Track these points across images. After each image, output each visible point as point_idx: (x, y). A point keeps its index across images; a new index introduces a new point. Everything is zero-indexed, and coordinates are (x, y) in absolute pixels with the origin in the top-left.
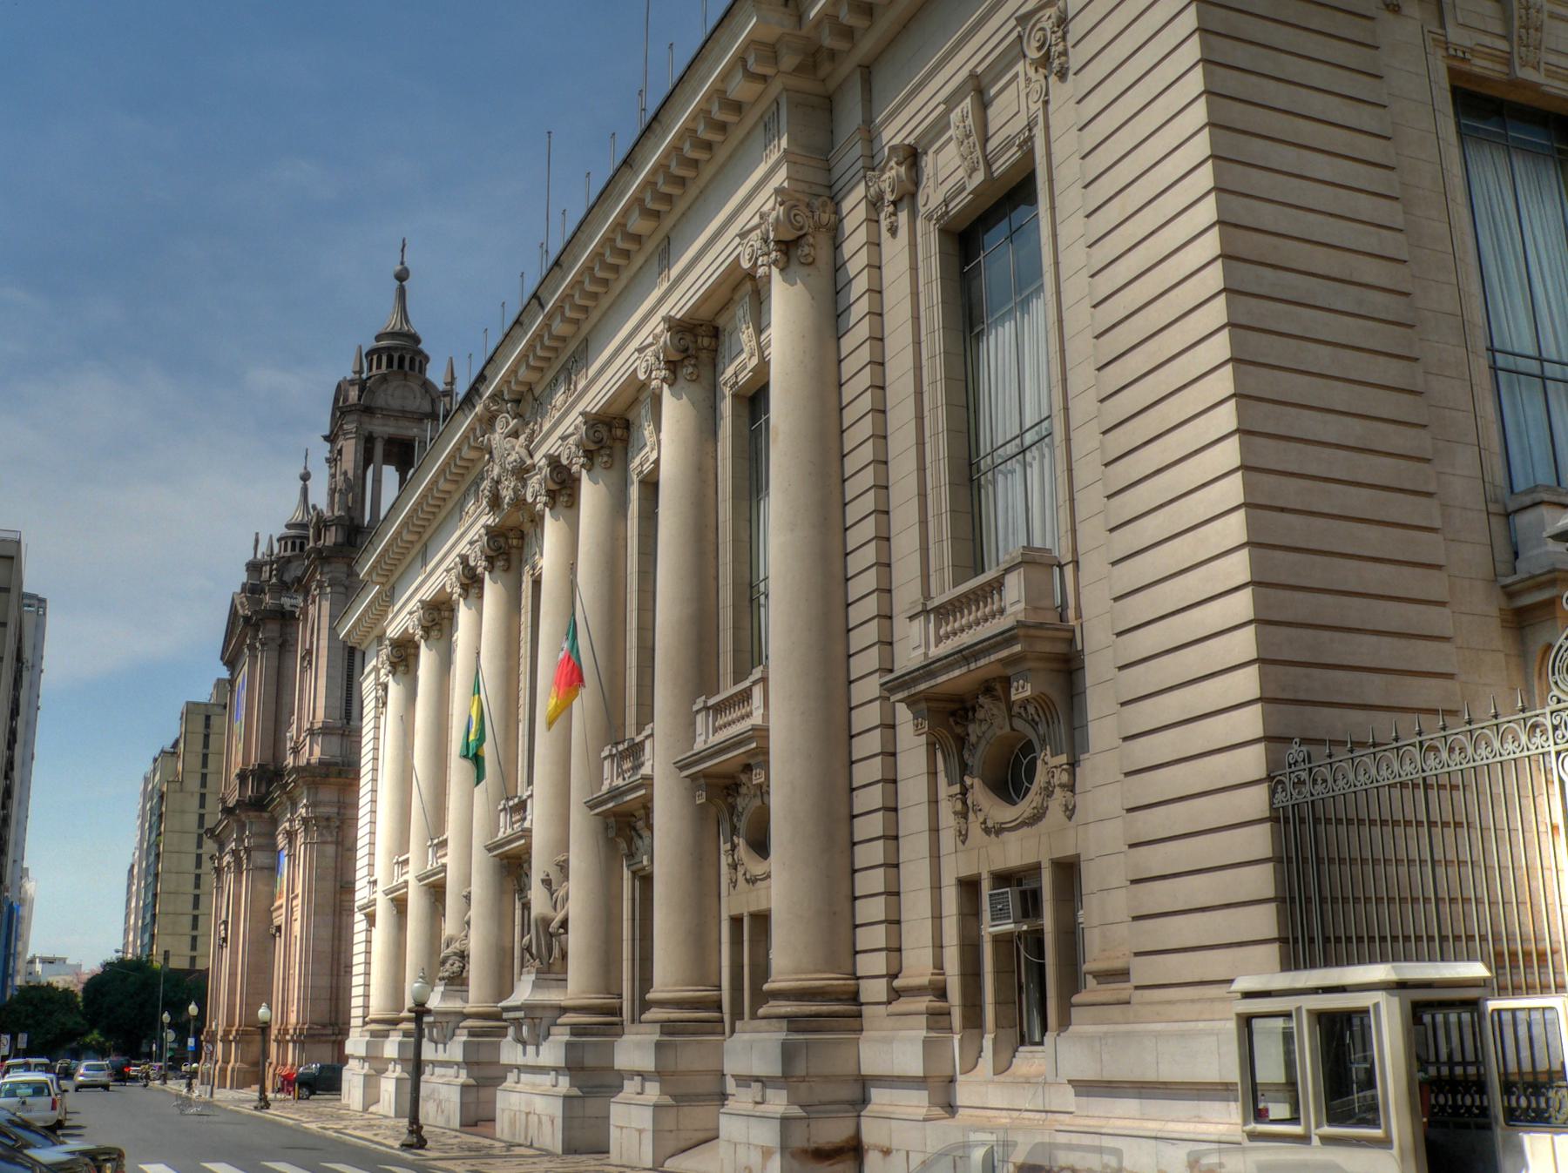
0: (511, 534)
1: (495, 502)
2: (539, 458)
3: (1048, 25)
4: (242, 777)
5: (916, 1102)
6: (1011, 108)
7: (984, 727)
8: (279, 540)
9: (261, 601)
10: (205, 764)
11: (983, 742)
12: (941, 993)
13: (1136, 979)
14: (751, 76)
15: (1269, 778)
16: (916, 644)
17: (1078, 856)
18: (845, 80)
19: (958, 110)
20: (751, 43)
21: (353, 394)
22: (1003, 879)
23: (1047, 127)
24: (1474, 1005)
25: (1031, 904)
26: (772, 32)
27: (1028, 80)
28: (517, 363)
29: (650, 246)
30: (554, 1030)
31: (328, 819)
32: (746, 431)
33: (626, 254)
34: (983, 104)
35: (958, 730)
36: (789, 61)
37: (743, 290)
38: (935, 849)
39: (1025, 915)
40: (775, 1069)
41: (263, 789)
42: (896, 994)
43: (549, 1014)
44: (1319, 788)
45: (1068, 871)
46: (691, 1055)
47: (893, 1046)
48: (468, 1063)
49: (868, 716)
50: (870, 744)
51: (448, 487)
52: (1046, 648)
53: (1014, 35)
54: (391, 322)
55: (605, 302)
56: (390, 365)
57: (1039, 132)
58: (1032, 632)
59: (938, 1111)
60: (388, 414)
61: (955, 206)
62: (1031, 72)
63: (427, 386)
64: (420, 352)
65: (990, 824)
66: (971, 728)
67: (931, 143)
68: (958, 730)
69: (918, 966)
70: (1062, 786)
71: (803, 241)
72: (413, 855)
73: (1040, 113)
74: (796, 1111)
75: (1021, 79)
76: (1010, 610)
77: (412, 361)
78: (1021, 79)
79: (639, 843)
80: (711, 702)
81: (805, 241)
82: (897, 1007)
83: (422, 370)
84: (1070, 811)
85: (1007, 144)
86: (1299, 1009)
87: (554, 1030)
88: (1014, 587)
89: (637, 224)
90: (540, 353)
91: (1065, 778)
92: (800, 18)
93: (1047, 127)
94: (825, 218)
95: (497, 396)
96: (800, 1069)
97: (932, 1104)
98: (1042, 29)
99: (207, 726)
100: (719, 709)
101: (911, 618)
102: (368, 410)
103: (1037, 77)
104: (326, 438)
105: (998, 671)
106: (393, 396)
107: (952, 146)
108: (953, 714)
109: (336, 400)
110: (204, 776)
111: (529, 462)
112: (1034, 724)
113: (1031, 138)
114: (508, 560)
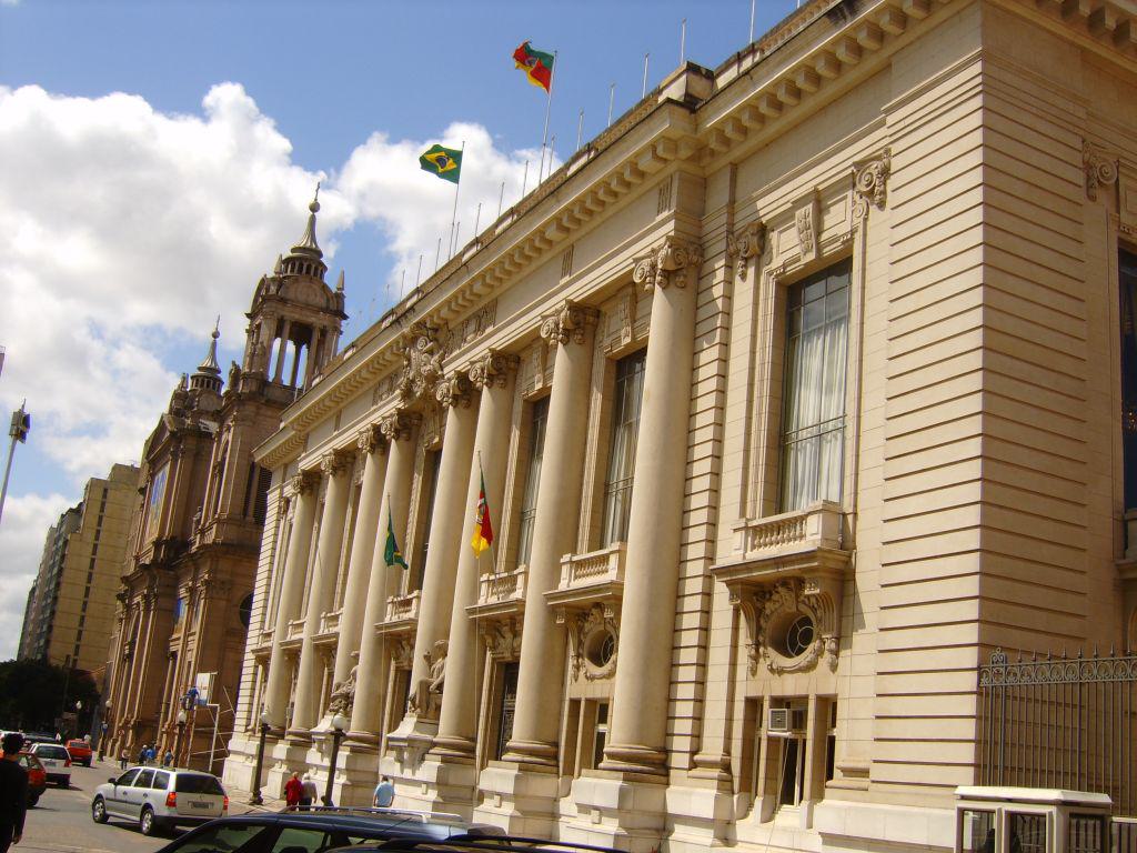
0: (414, 416)
1: (407, 394)
2: (449, 371)
3: (875, 173)
4: (157, 544)
5: (705, 836)
6: (839, 220)
7: (777, 605)
8: (192, 377)
9: (184, 423)
10: (99, 524)
11: (776, 614)
12: (727, 767)
13: (873, 776)
14: (656, 157)
15: (979, 668)
16: (732, 550)
17: (836, 695)
18: (719, 170)
19: (803, 210)
20: (662, 137)
21: (273, 289)
22: (778, 702)
23: (865, 235)
24: (1102, 818)
25: (799, 721)
26: (677, 134)
27: (854, 202)
28: (442, 305)
29: (558, 249)
30: (427, 756)
31: (223, 583)
32: (613, 383)
33: (539, 250)
34: (820, 211)
35: (759, 605)
36: (685, 153)
37: (627, 293)
38: (727, 672)
39: (794, 726)
40: (613, 803)
41: (172, 555)
42: (694, 765)
43: (423, 745)
44: (1011, 678)
45: (828, 705)
46: (457, 776)
47: (691, 796)
48: (441, 783)
49: (694, 586)
50: (692, 604)
51: (368, 376)
52: (831, 565)
53: (849, 171)
54: (302, 241)
55: (516, 278)
56: (300, 270)
57: (858, 237)
58: (827, 555)
59: (718, 842)
60: (296, 304)
61: (791, 270)
62: (857, 197)
63: (325, 287)
64: (322, 264)
65: (774, 667)
66: (768, 605)
67: (778, 225)
68: (759, 605)
69: (712, 749)
70: (831, 651)
71: (680, 272)
72: (308, 619)
73: (861, 226)
74: (623, 832)
75: (849, 200)
76: (808, 538)
77: (316, 269)
78: (849, 200)
79: (502, 641)
80: (575, 558)
81: (685, 269)
82: (694, 772)
83: (322, 276)
84: (834, 667)
85: (834, 239)
86: (1000, 810)
87: (427, 756)
88: (814, 526)
89: (552, 234)
90: (460, 301)
91: (833, 646)
92: (696, 130)
93: (865, 235)
94: (695, 258)
95: (421, 324)
96: (629, 805)
97: (715, 837)
98: (870, 173)
99: (105, 496)
100: (580, 564)
101: (735, 530)
102: (283, 301)
103: (862, 202)
104: (248, 315)
105: (797, 574)
106: (301, 291)
107: (794, 231)
108: (756, 594)
109: (259, 289)
110: (98, 532)
111: (440, 373)
112: (813, 609)
113: (852, 239)
114: (409, 434)
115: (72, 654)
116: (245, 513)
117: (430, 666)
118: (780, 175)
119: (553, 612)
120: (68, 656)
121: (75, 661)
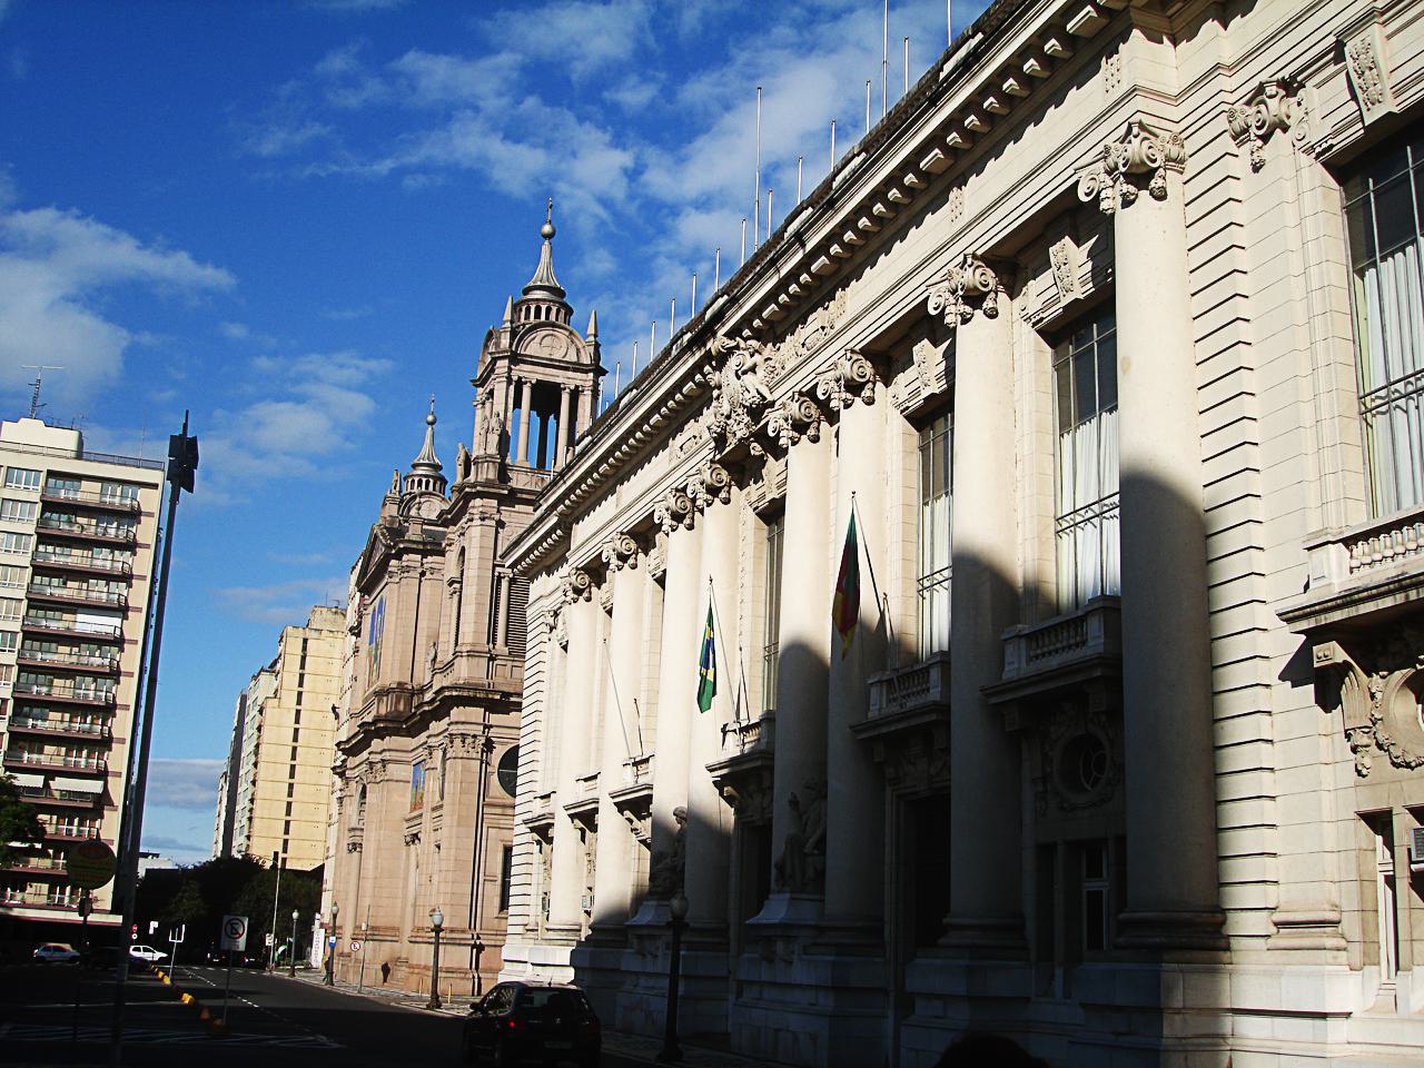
76: (1090, 643)
115: (280, 850)
116: (492, 638)
117: (800, 817)
118: (205, 758)
119: (996, 713)
120: (276, 854)
121: (284, 860)
